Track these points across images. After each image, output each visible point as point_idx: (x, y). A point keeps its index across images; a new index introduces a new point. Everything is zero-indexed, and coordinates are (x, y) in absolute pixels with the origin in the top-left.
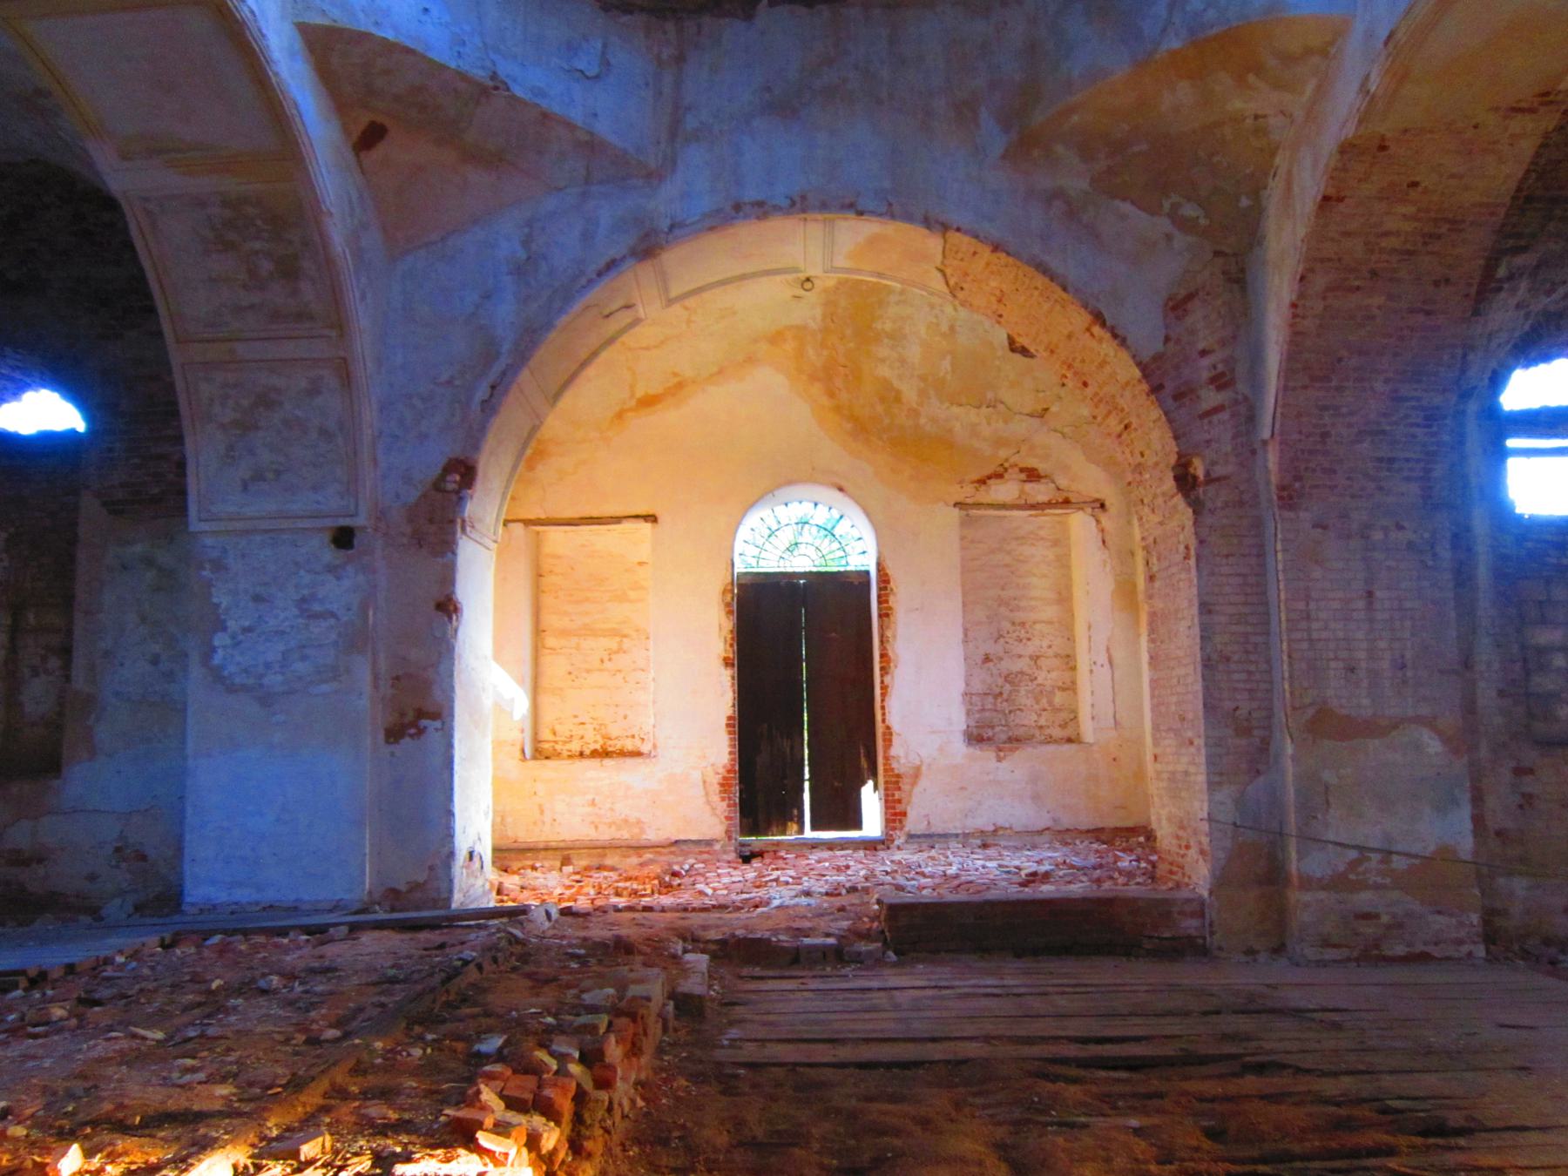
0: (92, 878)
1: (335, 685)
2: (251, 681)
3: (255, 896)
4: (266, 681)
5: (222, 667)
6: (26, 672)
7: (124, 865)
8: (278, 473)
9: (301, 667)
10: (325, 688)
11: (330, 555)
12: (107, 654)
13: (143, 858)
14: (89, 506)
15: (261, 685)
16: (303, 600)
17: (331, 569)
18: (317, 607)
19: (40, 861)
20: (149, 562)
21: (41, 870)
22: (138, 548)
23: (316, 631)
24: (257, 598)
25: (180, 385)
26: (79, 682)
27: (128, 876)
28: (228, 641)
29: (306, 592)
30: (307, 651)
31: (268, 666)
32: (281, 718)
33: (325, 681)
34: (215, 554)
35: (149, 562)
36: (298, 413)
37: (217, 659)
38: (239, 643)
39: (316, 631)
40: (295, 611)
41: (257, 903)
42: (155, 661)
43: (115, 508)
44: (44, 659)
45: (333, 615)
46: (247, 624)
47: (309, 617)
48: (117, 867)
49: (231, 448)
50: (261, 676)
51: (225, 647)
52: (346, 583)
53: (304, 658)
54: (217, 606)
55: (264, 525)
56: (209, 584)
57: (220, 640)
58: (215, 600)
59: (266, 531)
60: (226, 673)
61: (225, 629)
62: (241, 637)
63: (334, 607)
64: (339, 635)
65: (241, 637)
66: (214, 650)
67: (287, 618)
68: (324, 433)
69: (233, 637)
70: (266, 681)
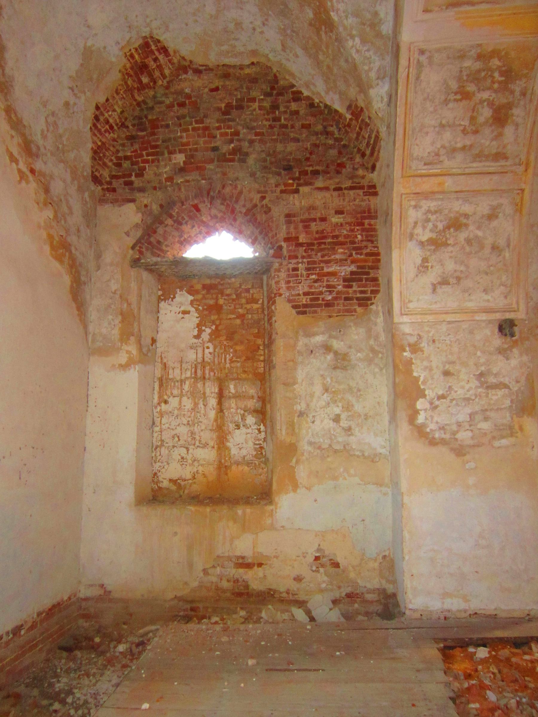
0: (298, 579)
1: (512, 440)
2: (447, 436)
3: (463, 606)
4: (459, 436)
5: (424, 425)
6: (232, 426)
7: (322, 570)
8: (459, 279)
9: (485, 426)
10: (504, 442)
11: (497, 341)
12: (301, 414)
13: (336, 565)
14: (283, 309)
15: (456, 439)
16: (481, 375)
17: (501, 351)
18: (492, 380)
19: (260, 565)
20: (328, 348)
21: (260, 572)
22: (319, 339)
23: (494, 398)
24: (447, 373)
25: (395, 208)
26: (282, 433)
27: (325, 578)
28: (428, 406)
29: (483, 368)
30: (488, 413)
31: (459, 425)
32: (472, 465)
33: (502, 437)
34: (413, 340)
35: (328, 348)
36: (480, 234)
37: (421, 419)
38: (436, 407)
39: (494, 398)
40: (477, 383)
41: (465, 611)
42: (337, 419)
43: (301, 310)
44: (243, 418)
45: (506, 386)
46: (440, 393)
47: (488, 388)
48: (318, 571)
49: (425, 260)
50: (454, 433)
51: (425, 410)
52: (514, 362)
53: (486, 419)
54: (417, 379)
55: (449, 318)
56: (410, 362)
57: (420, 404)
58: (415, 374)
59: (449, 323)
60: (428, 430)
61: (424, 396)
62: (437, 403)
63: (506, 380)
64: (512, 401)
65: (437, 403)
66: (416, 412)
67: (471, 388)
68: (494, 248)
69: (431, 403)
70: (459, 436)
